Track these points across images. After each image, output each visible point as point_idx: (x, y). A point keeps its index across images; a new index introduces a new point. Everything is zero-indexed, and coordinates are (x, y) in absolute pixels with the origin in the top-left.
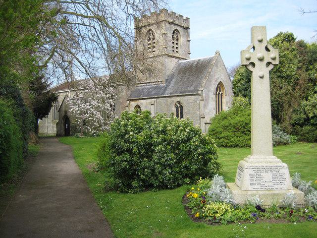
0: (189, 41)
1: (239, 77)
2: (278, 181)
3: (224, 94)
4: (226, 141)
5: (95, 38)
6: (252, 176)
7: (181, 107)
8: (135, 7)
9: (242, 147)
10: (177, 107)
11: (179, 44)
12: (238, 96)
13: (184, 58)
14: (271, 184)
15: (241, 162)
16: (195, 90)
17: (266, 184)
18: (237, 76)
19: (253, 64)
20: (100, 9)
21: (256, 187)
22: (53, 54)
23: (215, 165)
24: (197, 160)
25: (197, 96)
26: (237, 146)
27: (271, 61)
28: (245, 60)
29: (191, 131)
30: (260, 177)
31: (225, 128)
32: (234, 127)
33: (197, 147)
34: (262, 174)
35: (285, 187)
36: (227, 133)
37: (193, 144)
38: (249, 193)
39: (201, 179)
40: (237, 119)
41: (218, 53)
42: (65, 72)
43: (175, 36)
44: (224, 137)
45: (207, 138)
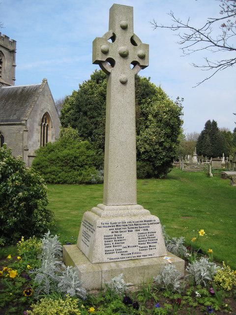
0: (14, 80)
1: (69, 106)
2: (147, 245)
3: (50, 126)
4: (53, 177)
6: (107, 238)
9: (71, 183)
12: (66, 126)
13: (9, 84)
14: (136, 250)
15: (88, 214)
16: (19, 119)
17: (130, 250)
18: (66, 105)
19: (112, 62)
23: (44, 214)
24: (16, 209)
25: (20, 126)
26: (65, 182)
27: (137, 60)
28: (100, 53)
29: (9, 164)
30: (121, 240)
31: (52, 161)
32: (62, 161)
33: (18, 189)
34: (123, 235)
35: (156, 252)
36: (54, 168)
37: (10, 184)
38: (105, 268)
39: (23, 240)
40: (66, 151)
44: (50, 172)
45: (32, 175)
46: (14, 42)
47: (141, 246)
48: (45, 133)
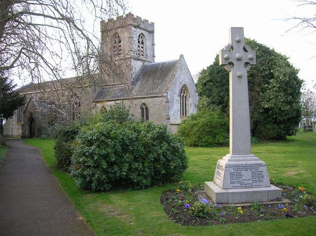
2: (257, 179)
3: (188, 96)
5: (63, 40)
7: (147, 108)
8: (103, 10)
10: (142, 109)
11: (144, 48)
14: (250, 182)
16: (160, 92)
17: (246, 182)
20: (69, 11)
21: (236, 185)
22: (19, 56)
27: (248, 61)
30: (240, 176)
34: (242, 172)
41: (182, 56)
42: (31, 73)
43: (141, 40)
46: (153, 24)
47: (254, 179)
48: (184, 103)
